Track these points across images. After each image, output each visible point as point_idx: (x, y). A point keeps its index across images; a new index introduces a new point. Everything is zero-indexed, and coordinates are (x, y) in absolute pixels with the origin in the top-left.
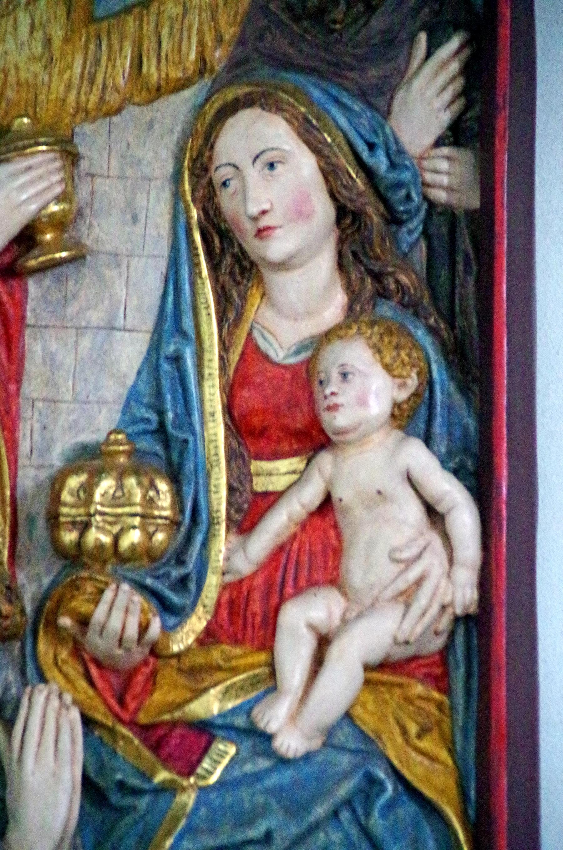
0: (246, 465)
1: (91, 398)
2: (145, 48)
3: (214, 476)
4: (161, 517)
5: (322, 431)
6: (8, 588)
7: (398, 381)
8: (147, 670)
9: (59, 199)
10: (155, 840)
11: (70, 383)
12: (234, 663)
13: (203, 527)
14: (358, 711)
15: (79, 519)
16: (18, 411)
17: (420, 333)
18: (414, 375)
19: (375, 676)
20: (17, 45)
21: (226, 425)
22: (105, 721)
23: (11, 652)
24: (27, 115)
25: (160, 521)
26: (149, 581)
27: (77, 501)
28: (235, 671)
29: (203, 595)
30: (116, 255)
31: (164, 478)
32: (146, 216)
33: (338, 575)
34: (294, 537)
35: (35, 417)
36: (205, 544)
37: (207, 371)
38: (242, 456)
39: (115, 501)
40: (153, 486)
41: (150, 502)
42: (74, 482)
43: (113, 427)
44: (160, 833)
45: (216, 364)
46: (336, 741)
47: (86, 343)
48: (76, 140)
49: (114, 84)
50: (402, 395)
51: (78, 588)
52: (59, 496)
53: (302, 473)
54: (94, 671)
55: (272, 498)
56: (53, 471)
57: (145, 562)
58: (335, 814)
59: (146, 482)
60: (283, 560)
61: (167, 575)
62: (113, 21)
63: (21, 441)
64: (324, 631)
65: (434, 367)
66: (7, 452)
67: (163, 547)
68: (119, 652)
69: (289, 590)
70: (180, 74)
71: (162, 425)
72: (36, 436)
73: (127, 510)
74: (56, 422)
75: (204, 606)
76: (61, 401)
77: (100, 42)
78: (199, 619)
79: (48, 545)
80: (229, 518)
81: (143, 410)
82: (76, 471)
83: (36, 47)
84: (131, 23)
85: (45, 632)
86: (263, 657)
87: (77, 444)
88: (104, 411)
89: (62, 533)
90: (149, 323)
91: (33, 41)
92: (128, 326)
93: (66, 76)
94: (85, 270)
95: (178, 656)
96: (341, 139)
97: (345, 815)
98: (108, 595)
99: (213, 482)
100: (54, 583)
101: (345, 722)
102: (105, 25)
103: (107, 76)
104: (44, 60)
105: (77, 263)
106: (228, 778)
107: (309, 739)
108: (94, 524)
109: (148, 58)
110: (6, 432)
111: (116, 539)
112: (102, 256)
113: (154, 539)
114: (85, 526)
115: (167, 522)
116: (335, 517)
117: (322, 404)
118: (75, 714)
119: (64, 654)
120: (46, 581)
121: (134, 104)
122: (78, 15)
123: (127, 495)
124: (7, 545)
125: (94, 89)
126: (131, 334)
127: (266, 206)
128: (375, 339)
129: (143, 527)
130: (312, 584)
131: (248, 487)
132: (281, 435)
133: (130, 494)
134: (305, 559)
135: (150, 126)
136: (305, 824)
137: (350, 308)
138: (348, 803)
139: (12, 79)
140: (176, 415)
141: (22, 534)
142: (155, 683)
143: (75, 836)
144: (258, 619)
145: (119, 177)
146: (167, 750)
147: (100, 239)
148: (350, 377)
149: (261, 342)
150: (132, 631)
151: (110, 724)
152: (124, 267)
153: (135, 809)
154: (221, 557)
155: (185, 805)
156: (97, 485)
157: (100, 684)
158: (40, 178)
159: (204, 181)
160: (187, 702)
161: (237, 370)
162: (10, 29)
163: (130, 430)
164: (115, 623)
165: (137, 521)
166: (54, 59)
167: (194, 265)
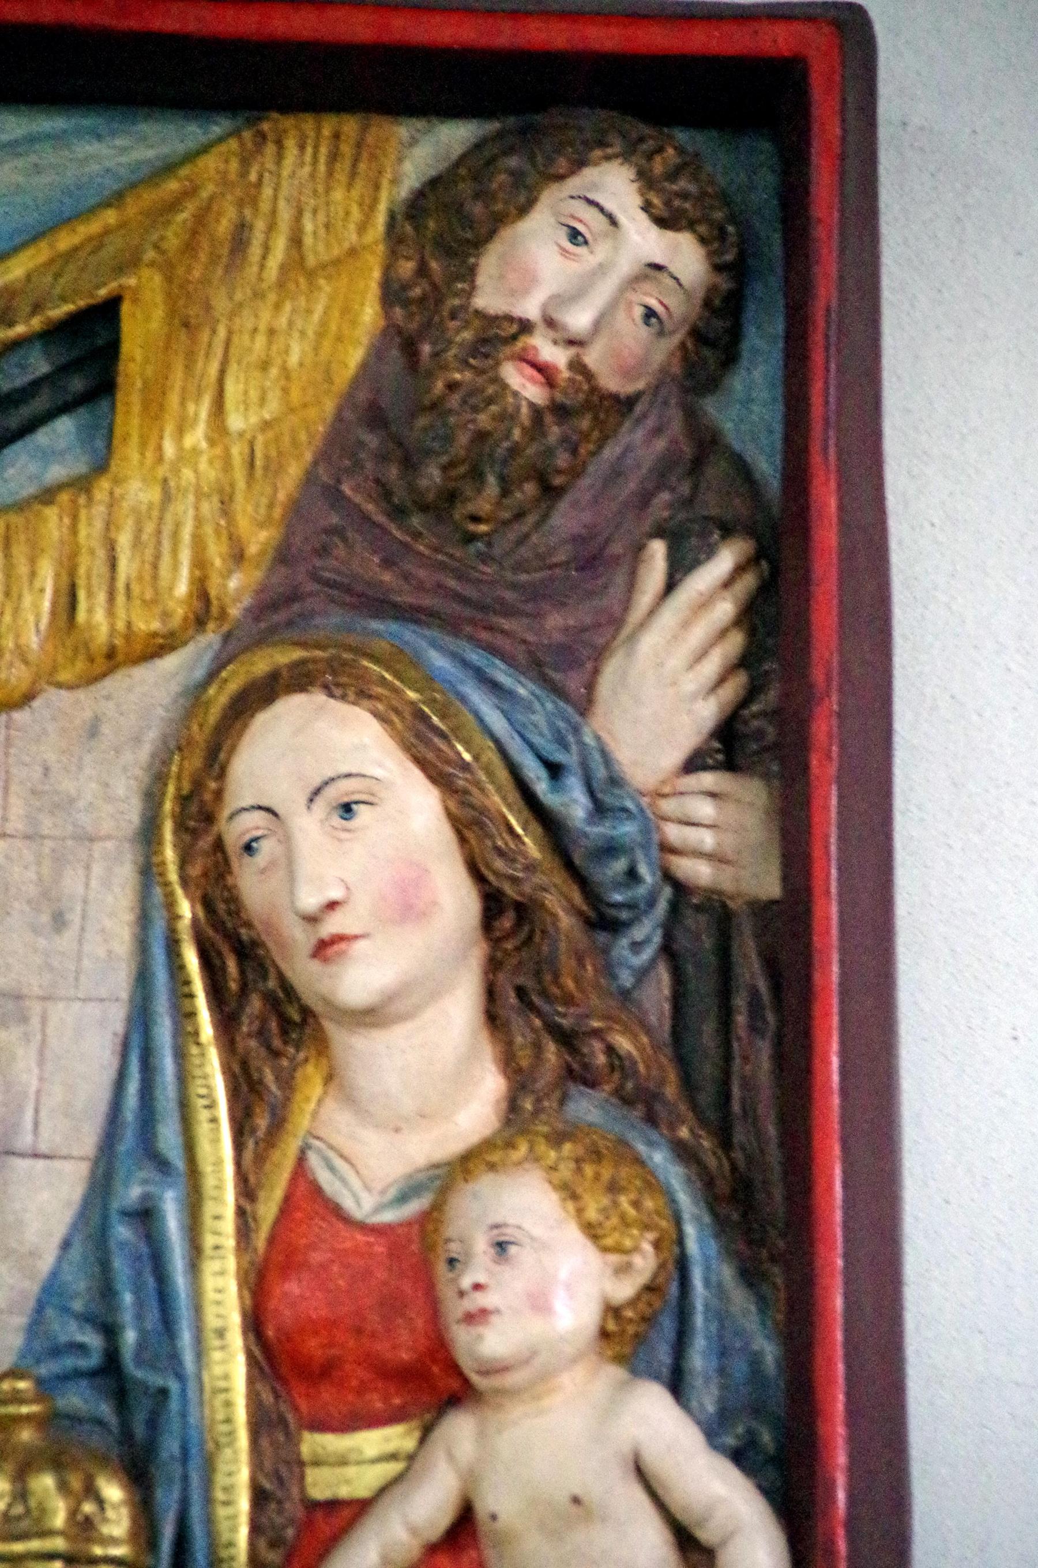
0: (292, 1441)
2: (82, 571)
3: (222, 1467)
5: (454, 1368)
7: (614, 1258)
17: (659, 1157)
18: (647, 1247)
32: (84, 917)
37: (209, 1241)
38: (282, 1421)
40: (91, 1492)
45: (228, 1225)
49: (18, 646)
50: (624, 1290)
55: (346, 1513)
59: (76, 1482)
62: (16, 520)
65: (690, 1230)
70: (156, 625)
73: (35, 1545)
81: (73, 1326)
90: (88, 1141)
92: (43, 1147)
96: (491, 756)
109: (90, 594)
116: (480, 1556)
117: (454, 1309)
121: (59, 685)
123: (35, 1514)
126: (48, 1162)
127: (335, 893)
128: (566, 1171)
131: (295, 1491)
133: (44, 1511)
135: (93, 731)
137: (512, 1106)
140: (143, 1334)
148: (513, 1250)
149: (324, 1178)
159: (205, 843)
161: (272, 1240)
167: (185, 1016)
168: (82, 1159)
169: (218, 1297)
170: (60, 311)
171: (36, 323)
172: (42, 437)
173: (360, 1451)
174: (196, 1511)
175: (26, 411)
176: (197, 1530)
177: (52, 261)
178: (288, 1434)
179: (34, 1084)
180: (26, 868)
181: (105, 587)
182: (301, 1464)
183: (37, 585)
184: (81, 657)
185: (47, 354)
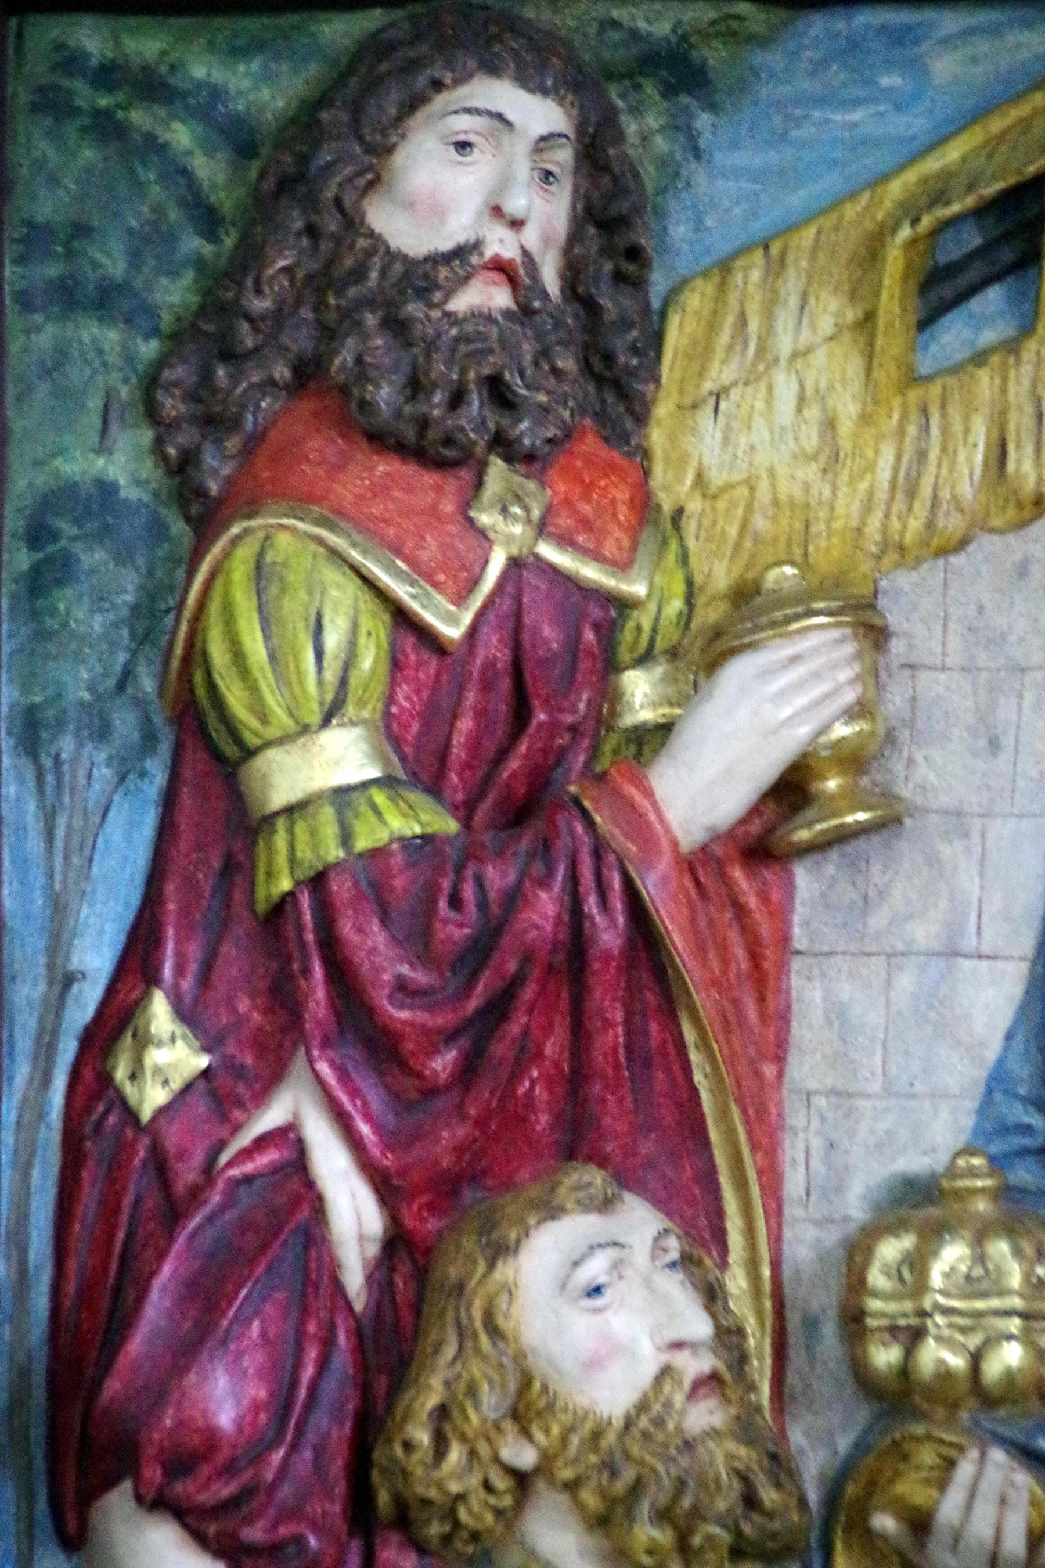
1: (919, 1087)
2: (1011, 427)
6: (774, 1457)
9: (851, 714)
11: (878, 1059)
15: (902, 1322)
16: (780, 1115)
20: (772, 431)
24: (793, 563)
27: (899, 1286)
30: (959, 814)
32: (1017, 740)
35: (812, 1128)
43: (962, 1140)
47: (906, 981)
48: (882, 602)
49: (954, 496)
51: (905, 1457)
52: (862, 1281)
56: (852, 1228)
62: (951, 381)
63: (788, 1169)
66: (763, 1194)
72: (816, 1163)
73: (995, 1303)
74: (852, 1133)
77: (928, 420)
79: (844, 1373)
82: (895, 1229)
83: (809, 437)
84: (985, 380)
85: (848, 1546)
87: (893, 1176)
88: (944, 1114)
91: (803, 426)
92: (986, 949)
93: (863, 486)
94: (902, 845)
98: (965, 1470)
100: (861, 1448)
102: (935, 390)
103: (941, 480)
104: (823, 459)
105: (885, 832)
109: (1018, 447)
110: (760, 1155)
111: (976, 1359)
112: (934, 818)
114: (914, 1336)
120: (844, 1443)
121: (992, 531)
122: (887, 373)
123: (993, 1276)
124: (768, 1373)
125: (917, 505)
126: (992, 962)
133: (1000, 1272)
135: (1022, 570)
139: (763, 495)
141: (797, 1356)
145: (963, 669)
147: (928, 787)
152: (976, 838)
156: (935, 1254)
158: (816, 676)
162: (760, 405)
163: (994, 1149)
165: (1014, 1325)
166: (842, 454)
168: (1021, 959)
170: (991, 189)
171: (970, 201)
172: (975, 304)
175: (963, 281)
177: (986, 142)
179: (977, 891)
180: (965, 697)
181: (1033, 440)
183: (971, 440)
184: (1012, 504)
185: (981, 229)
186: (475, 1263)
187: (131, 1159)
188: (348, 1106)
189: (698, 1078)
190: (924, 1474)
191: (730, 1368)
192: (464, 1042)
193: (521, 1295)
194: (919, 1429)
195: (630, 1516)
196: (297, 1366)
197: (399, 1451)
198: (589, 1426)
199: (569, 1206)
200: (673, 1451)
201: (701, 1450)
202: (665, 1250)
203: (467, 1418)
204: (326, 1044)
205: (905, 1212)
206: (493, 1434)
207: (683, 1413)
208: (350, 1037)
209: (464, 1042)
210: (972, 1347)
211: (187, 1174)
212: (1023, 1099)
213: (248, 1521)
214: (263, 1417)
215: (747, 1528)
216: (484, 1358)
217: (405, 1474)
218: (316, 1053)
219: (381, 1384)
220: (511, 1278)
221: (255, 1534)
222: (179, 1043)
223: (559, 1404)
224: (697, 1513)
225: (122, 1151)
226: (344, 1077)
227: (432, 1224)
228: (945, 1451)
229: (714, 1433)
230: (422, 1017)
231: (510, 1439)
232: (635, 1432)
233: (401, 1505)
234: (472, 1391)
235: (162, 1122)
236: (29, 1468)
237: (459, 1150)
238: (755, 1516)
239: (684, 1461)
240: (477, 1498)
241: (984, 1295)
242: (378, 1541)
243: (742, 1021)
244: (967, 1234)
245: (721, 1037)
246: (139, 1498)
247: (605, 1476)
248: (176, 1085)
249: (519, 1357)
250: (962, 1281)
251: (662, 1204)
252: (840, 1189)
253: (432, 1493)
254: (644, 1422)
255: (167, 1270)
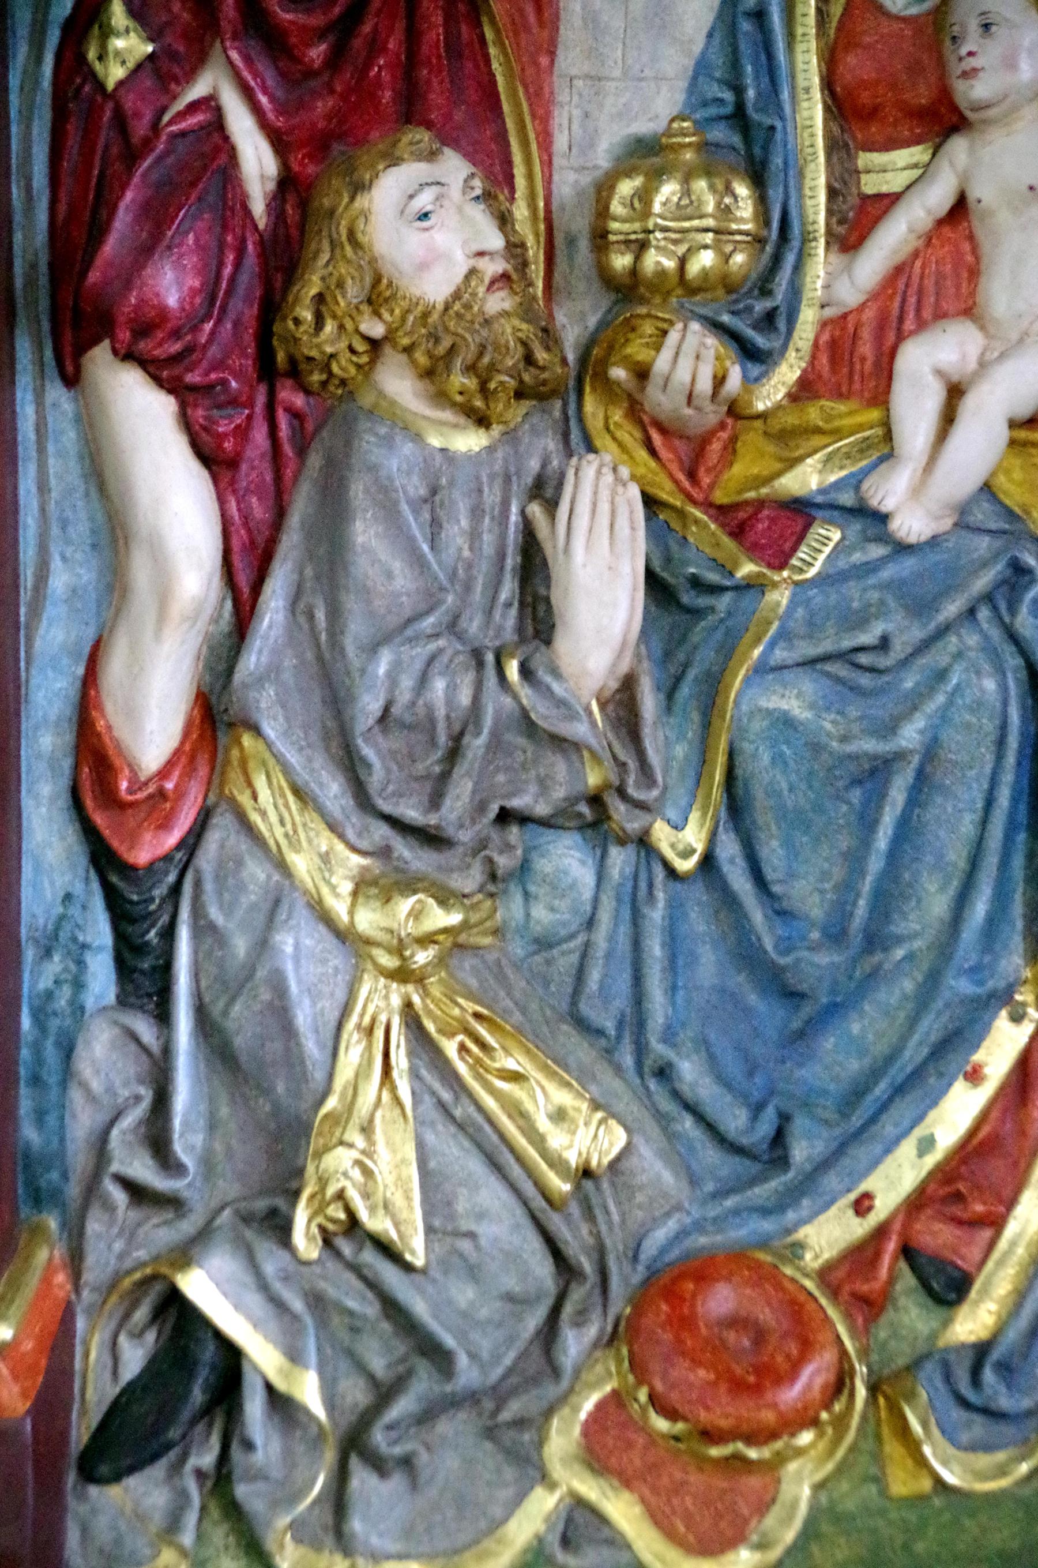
0: (852, 158)
1: (647, 72)
3: (809, 175)
4: (740, 232)
5: (955, 109)
6: (545, 330)
8: (724, 435)
10: (741, 649)
11: (619, 53)
12: (837, 423)
13: (796, 244)
14: (1001, 480)
15: (633, 237)
19: (1023, 434)
21: (825, 103)
22: (671, 500)
23: (550, 414)
25: (738, 238)
26: (725, 318)
28: (838, 434)
29: (796, 335)
31: (743, 179)
33: (975, 303)
34: (916, 254)
36: (798, 268)
37: (799, 31)
38: (846, 145)
39: (680, 212)
40: (729, 190)
41: (725, 212)
42: (626, 187)
43: (675, 113)
44: (748, 637)
45: (812, 20)
46: (971, 519)
52: (607, 208)
53: (927, 165)
54: (657, 438)
56: (598, 173)
57: (720, 292)
58: (971, 612)
59: (720, 186)
60: (901, 285)
61: (749, 309)
63: (556, 133)
64: (955, 378)
67: (743, 272)
68: (688, 412)
69: (909, 324)
71: (740, 107)
72: (575, 127)
73: (696, 223)
74: (601, 106)
75: (798, 350)
76: (608, 79)
78: (791, 367)
79: (594, 274)
80: (829, 233)
81: (715, 87)
82: (629, 174)
85: (594, 389)
86: (874, 414)
87: (629, 136)
88: (664, 89)
89: (613, 256)
95: (763, 416)
97: (984, 613)
98: (673, 336)
99: (808, 183)
100: (603, 325)
101: (984, 497)
106: (831, 571)
107: (937, 518)
108: (654, 242)
111: (683, 262)
113: (731, 261)
114: (641, 247)
115: (749, 238)
116: (970, 227)
117: (956, 69)
118: (634, 492)
119: (617, 415)
120: (592, 321)
123: (695, 204)
124: (542, 274)
129: (717, 247)
130: (940, 315)
131: (854, 191)
132: (899, 114)
133: (700, 202)
134: (930, 284)
136: (932, 626)
138: (988, 598)
140: (759, 94)
142: (734, 451)
143: (638, 645)
144: (868, 365)
146: (751, 537)
148: (994, 29)
150: (705, 385)
151: (678, 504)
153: (712, 609)
154: (819, 284)
155: (778, 604)
156: (657, 190)
157: (664, 454)
160: (779, 474)
161: (839, 29)
164: (683, 375)
165: (708, 238)
169: (805, 67)
173: (895, 163)
174: (793, 202)
176: (794, 212)
178: (849, 154)
182: (858, 172)
186: (341, 195)
187: (101, 118)
188: (252, 83)
189: (495, 66)
190: (644, 341)
191: (516, 269)
192: (331, 38)
193: (373, 218)
194: (643, 310)
195: (448, 369)
196: (221, 265)
197: (291, 324)
198: (420, 308)
199: (406, 156)
200: (477, 326)
201: (496, 326)
202: (472, 188)
203: (337, 303)
204: (235, 37)
205: (634, 161)
206: (354, 313)
207: (484, 300)
208: (251, 32)
209: (331, 38)
210: (680, 254)
211: (140, 129)
212: (719, 81)
213: (190, 369)
214: (198, 300)
215: (526, 377)
216: (349, 262)
217: (296, 340)
218: (228, 44)
219: (279, 279)
220: (366, 205)
221: (193, 378)
222: (132, 34)
223: (400, 293)
224: (492, 368)
225: (92, 113)
226: (248, 59)
227: (311, 169)
228: (661, 325)
229: (505, 314)
230: (302, 18)
231: (366, 317)
232: (451, 312)
233: (292, 361)
234: (340, 285)
235: (122, 92)
236: (39, 331)
237: (329, 117)
238: (532, 369)
239: (484, 333)
240: (345, 357)
241: (690, 218)
242: (278, 385)
243: (527, 29)
244: (679, 175)
245: (511, 34)
246: (115, 352)
247: (432, 341)
248: (131, 64)
249: (373, 261)
250: (673, 208)
251: (470, 157)
252: (592, 145)
253: (314, 353)
254: (457, 307)
255: (129, 195)
